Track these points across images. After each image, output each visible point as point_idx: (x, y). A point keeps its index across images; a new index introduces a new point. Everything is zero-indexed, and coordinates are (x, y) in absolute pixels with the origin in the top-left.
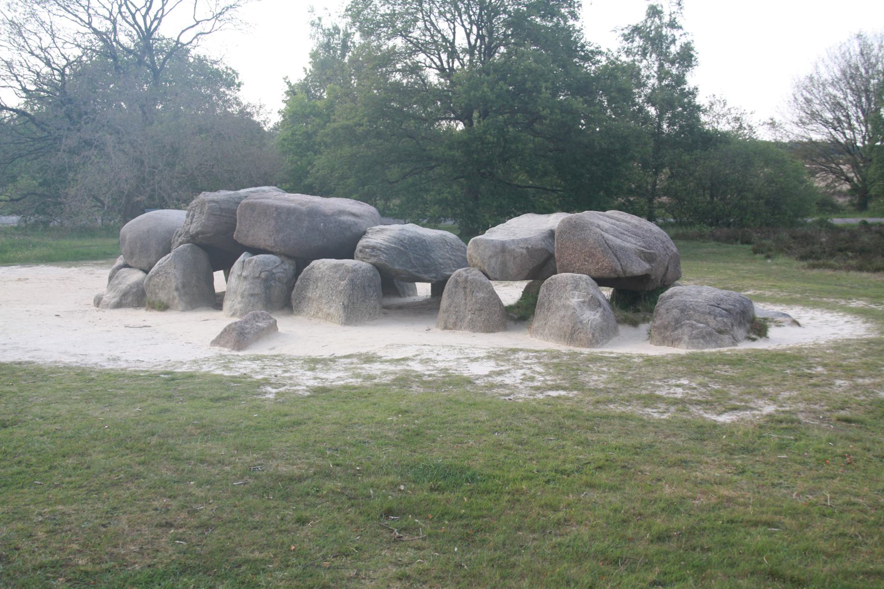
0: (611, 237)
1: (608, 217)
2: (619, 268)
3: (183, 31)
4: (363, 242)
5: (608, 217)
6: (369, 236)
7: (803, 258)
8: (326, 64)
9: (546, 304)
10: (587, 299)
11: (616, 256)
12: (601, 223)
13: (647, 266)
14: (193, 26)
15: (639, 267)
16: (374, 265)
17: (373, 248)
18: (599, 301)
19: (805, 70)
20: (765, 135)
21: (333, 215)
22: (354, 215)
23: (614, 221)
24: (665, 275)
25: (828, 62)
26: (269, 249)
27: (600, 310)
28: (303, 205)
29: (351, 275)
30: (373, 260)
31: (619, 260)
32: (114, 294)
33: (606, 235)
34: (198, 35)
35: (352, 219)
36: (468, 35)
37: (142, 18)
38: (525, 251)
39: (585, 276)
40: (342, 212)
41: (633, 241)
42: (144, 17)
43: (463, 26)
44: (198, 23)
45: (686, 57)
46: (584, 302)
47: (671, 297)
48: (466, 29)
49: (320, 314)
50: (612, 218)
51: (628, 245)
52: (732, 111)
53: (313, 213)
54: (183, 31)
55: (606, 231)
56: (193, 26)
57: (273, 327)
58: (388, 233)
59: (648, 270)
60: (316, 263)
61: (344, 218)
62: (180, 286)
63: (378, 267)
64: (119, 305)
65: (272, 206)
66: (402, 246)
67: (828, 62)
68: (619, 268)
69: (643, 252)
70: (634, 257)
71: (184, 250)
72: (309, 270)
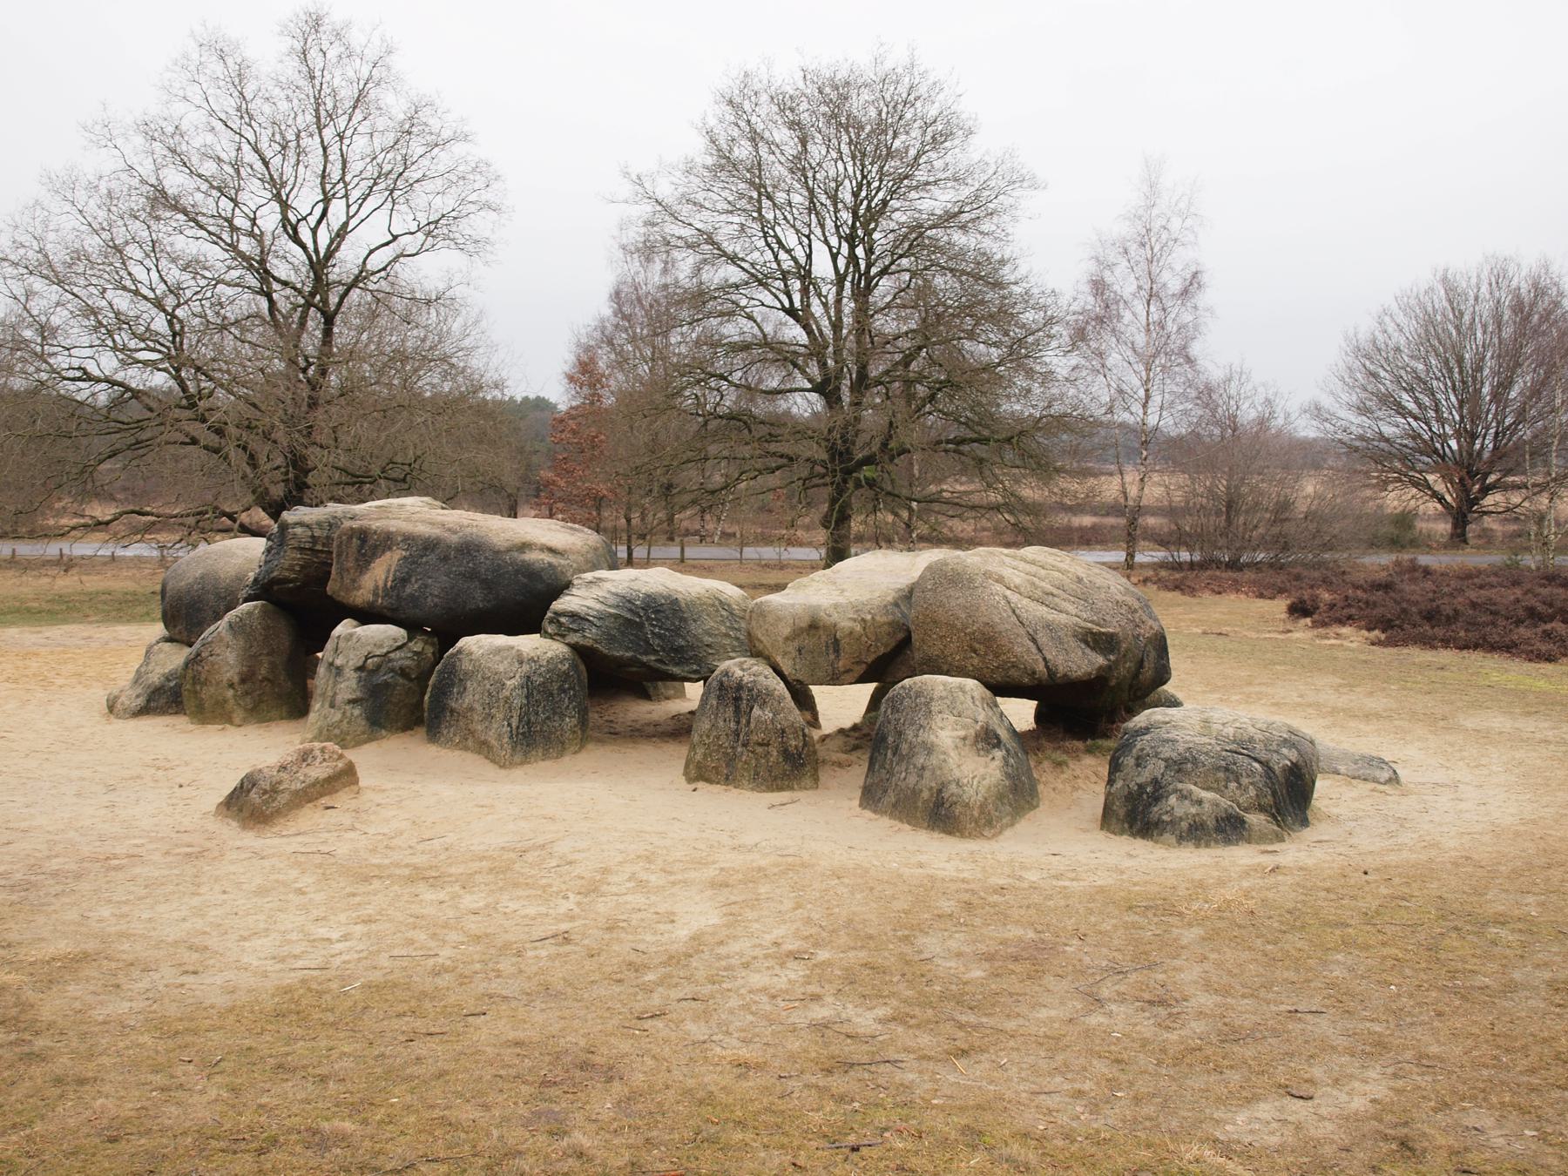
0: (1026, 601)
1: (1024, 560)
2: (1041, 667)
3: (372, 252)
4: (564, 603)
5: (1024, 560)
6: (574, 591)
7: (998, 285)
8: (646, 316)
9: (890, 739)
10: (972, 732)
11: (1034, 640)
12: (1007, 573)
13: (1100, 660)
14: (387, 244)
15: (1081, 663)
16: (574, 647)
17: (574, 616)
18: (997, 737)
19: (1366, 328)
20: (1307, 429)
21: (509, 550)
22: (551, 550)
23: (1033, 569)
24: (1136, 675)
25: (1401, 318)
26: (389, 614)
27: (999, 754)
28: (455, 533)
29: (526, 668)
30: (574, 638)
31: (1040, 650)
32: (139, 691)
33: (1014, 597)
34: (398, 257)
35: (547, 558)
36: (834, 257)
37: (310, 234)
38: (858, 628)
39: (971, 683)
40: (525, 546)
41: (1071, 608)
42: (314, 231)
43: (826, 242)
44: (395, 238)
45: (1192, 285)
46: (964, 739)
47: (1146, 730)
48: (830, 248)
49: (470, 743)
50: (1033, 563)
51: (1062, 618)
52: (1261, 389)
53: (470, 549)
54: (372, 252)
55: (1016, 589)
56: (387, 244)
57: (346, 776)
58: (608, 586)
59: (1100, 668)
60: (466, 642)
61: (532, 556)
62: (236, 679)
63: (582, 653)
64: (144, 711)
65: (398, 533)
66: (630, 610)
67: (1401, 318)
68: (1041, 667)
69: (1090, 632)
70: (1073, 643)
71: (250, 613)
72: (453, 655)
